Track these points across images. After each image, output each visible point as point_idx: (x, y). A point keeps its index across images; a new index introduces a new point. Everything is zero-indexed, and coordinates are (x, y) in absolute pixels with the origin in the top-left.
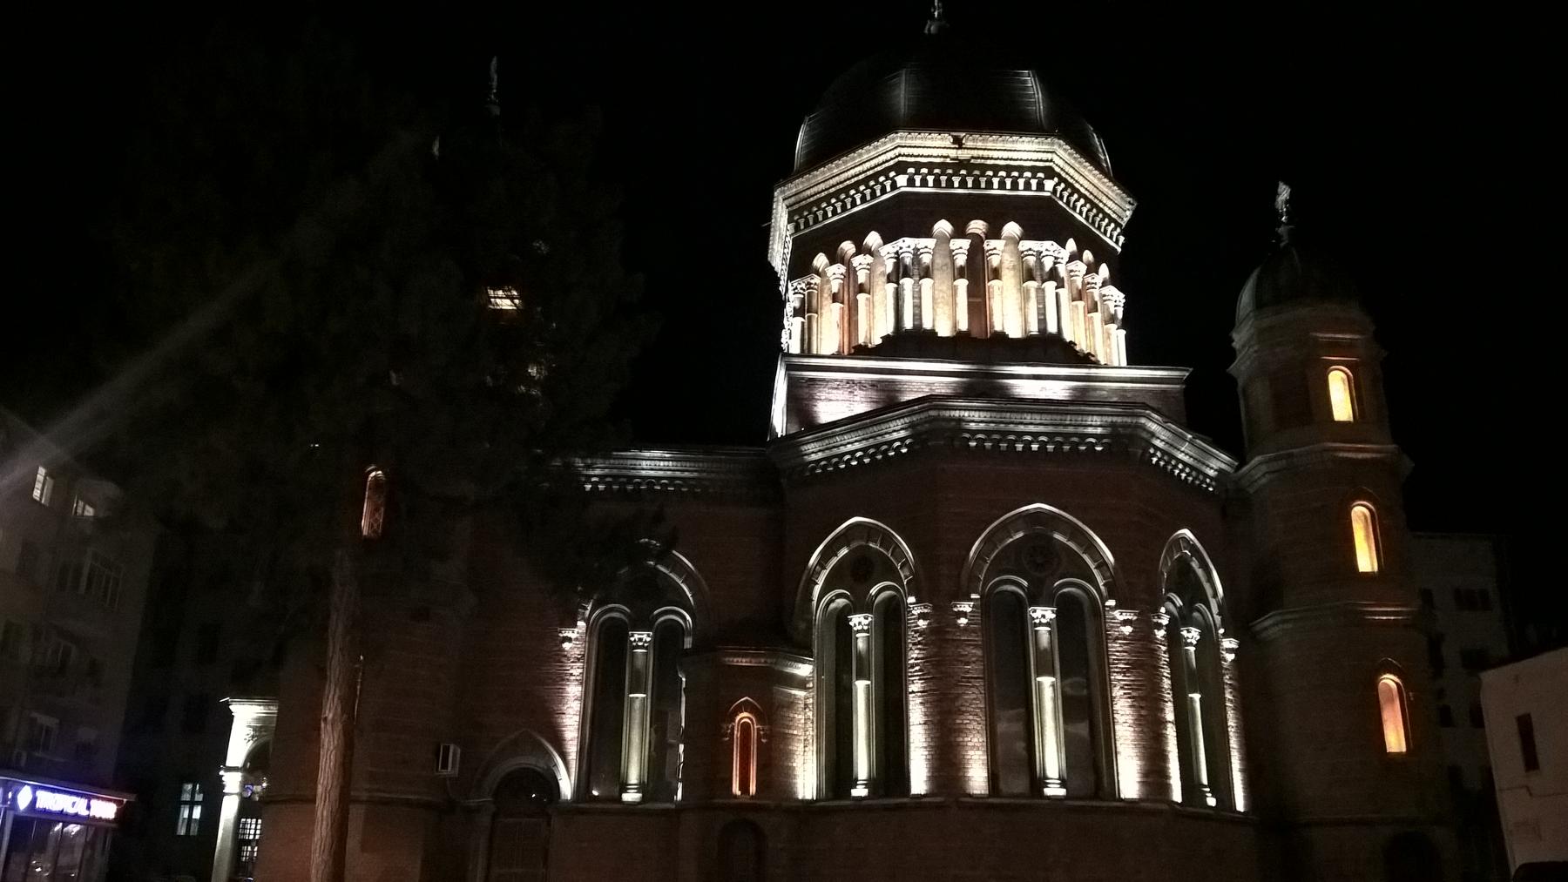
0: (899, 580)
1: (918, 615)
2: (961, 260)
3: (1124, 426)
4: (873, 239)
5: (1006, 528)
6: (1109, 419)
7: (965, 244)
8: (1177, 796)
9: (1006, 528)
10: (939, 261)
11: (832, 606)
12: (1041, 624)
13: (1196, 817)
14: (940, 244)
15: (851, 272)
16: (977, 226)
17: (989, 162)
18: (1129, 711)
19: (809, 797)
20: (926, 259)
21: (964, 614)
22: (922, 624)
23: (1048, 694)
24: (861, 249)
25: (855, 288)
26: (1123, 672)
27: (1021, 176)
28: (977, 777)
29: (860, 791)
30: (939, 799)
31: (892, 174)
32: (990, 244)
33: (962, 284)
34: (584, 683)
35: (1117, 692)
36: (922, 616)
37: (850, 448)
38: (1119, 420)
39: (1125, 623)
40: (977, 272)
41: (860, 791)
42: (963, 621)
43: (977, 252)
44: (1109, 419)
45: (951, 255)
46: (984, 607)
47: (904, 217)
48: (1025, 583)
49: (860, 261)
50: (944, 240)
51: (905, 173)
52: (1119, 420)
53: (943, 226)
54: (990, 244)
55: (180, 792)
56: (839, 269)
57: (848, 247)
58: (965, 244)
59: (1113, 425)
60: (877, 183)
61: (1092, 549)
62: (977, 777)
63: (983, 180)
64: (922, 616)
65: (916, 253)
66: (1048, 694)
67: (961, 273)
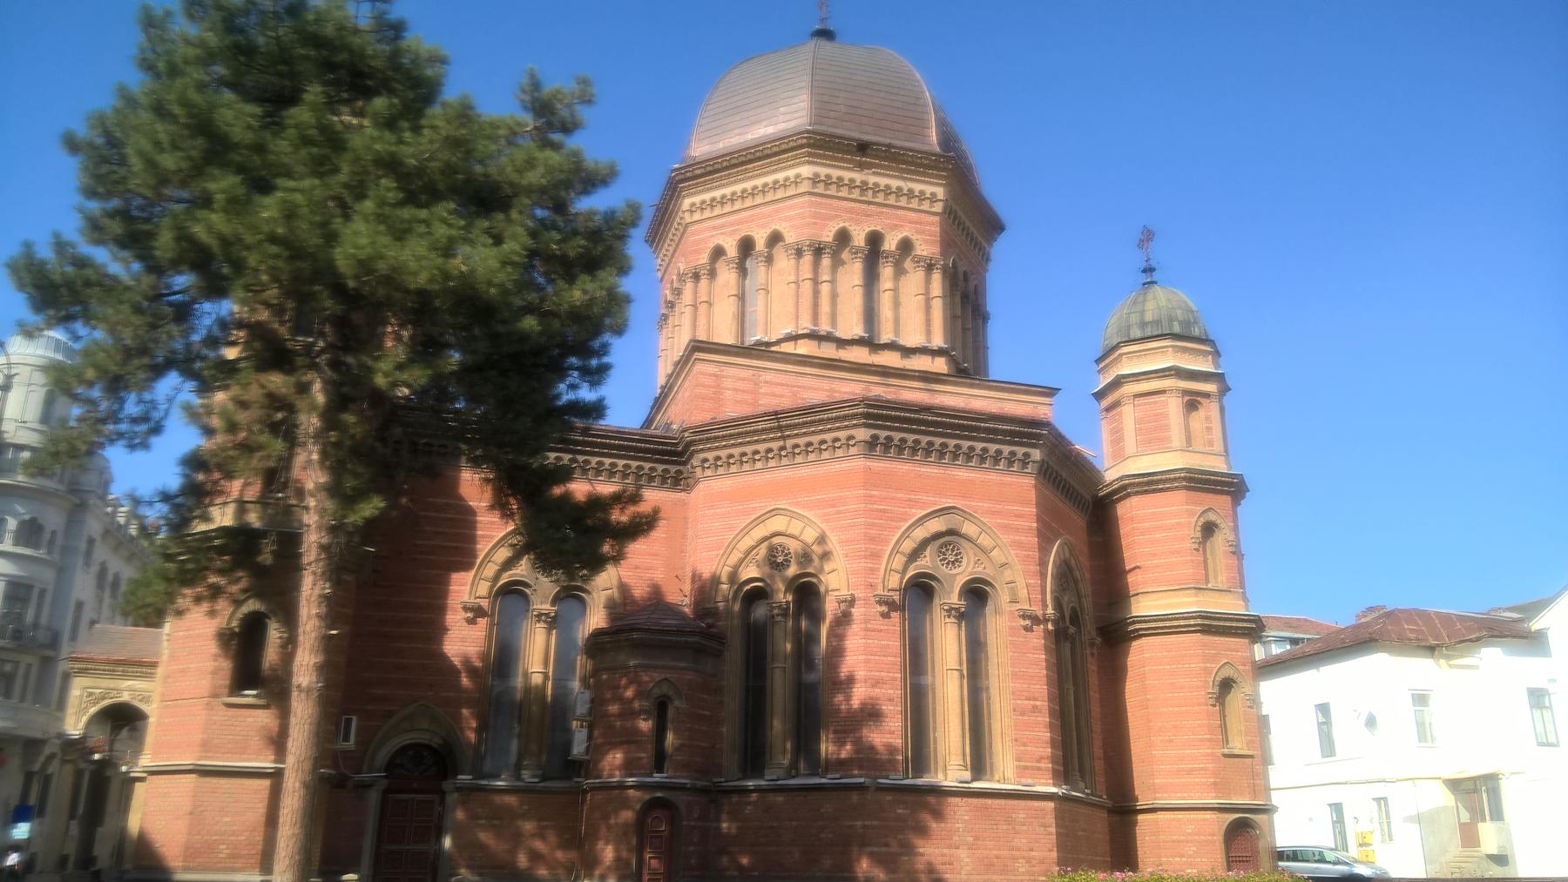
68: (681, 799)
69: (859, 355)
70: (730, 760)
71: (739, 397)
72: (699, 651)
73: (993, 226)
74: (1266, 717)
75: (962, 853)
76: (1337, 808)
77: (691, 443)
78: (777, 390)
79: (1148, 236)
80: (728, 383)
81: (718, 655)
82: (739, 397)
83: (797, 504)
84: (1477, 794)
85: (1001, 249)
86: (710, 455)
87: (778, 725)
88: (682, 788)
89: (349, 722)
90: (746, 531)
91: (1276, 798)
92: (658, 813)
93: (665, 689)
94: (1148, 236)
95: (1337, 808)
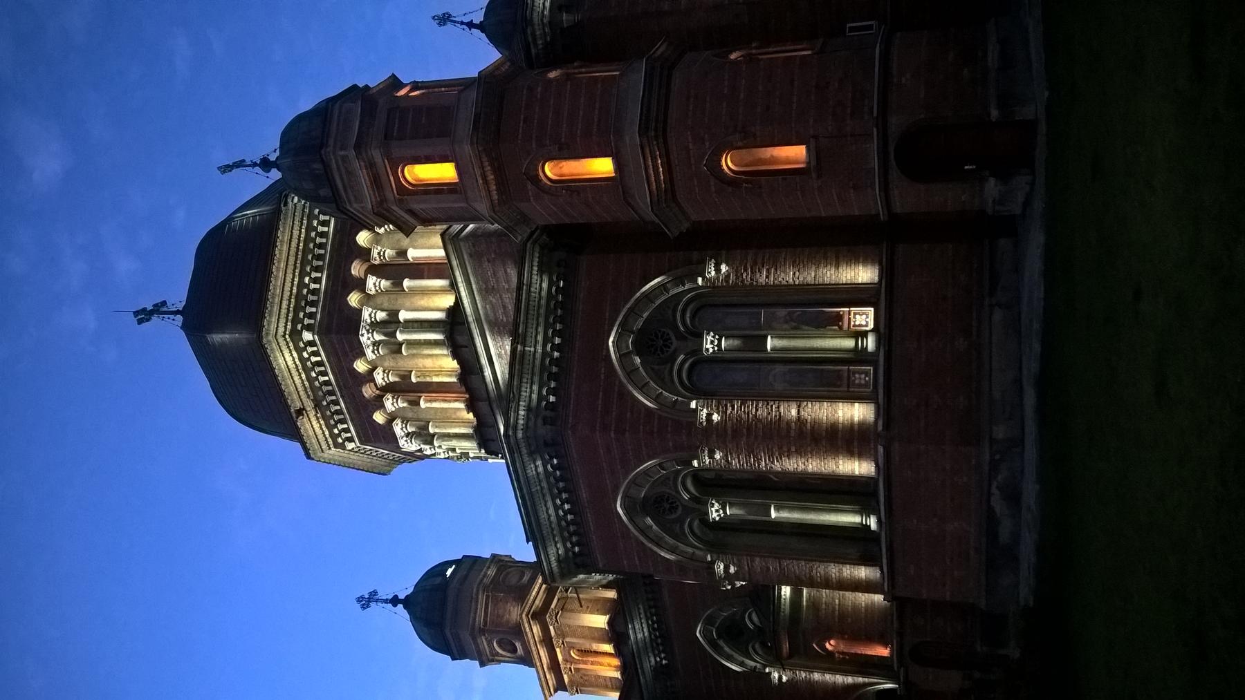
0: (678, 472)
1: (710, 459)
2: (385, 284)
3: (529, 445)
4: (360, 366)
5: (631, 372)
6: (526, 458)
7: (371, 281)
8: (878, 598)
9: (631, 372)
10: (386, 305)
11: (697, 531)
12: (719, 345)
13: (892, 584)
14: (369, 300)
15: (389, 388)
16: (357, 269)
17: (295, 291)
18: (793, 461)
19: (877, 271)
20: (381, 315)
21: (709, 415)
22: (718, 456)
23: (785, 515)
24: (369, 377)
25: (404, 387)
26: (759, 461)
27: (315, 229)
28: (857, 412)
29: (873, 523)
30: (881, 449)
31: (302, 345)
32: (376, 258)
33: (407, 283)
34: (775, 264)
35: (777, 466)
36: (711, 456)
37: (551, 511)
38: (524, 451)
39: (718, 270)
40: (398, 270)
41: (873, 523)
42: (716, 417)
43: (379, 270)
44: (526, 458)
45: (380, 293)
46: (704, 394)
47: (340, 330)
48: (682, 357)
49: (379, 377)
50: (368, 299)
51: (300, 333)
52: (524, 451)
53: (354, 299)
54: (376, 258)
55: (878, 342)
56: (390, 403)
57: (368, 391)
58: (371, 281)
59: (531, 454)
60: (309, 359)
61: (648, 296)
62: (857, 412)
63: (310, 298)
64: (711, 456)
65: (375, 326)
66: (785, 515)
67: (398, 284)
89: (852, 29)
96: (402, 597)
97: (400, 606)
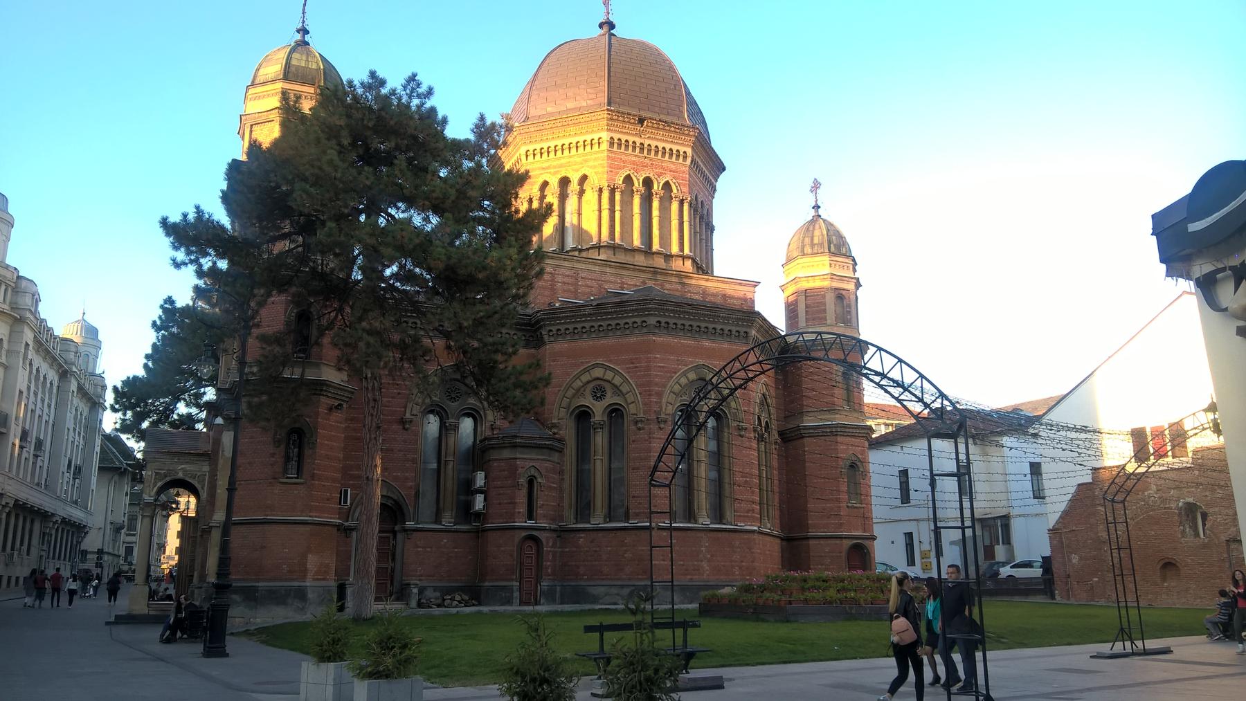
68: (543, 536)
69: (640, 260)
70: (569, 514)
71: (566, 287)
72: (551, 449)
73: (718, 167)
74: (1162, 261)
75: (705, 564)
76: (909, 536)
77: (543, 320)
78: (589, 283)
79: (816, 186)
80: (559, 279)
81: (560, 451)
82: (566, 287)
83: (610, 361)
84: (58, 570)
85: (722, 182)
86: (554, 329)
87: (55, 391)
88: (544, 529)
89: (346, 492)
90: (578, 377)
91: (877, 530)
92: (530, 543)
93: (533, 472)
94: (816, 186)
95: (909, 536)
96: (307, 38)
97: (298, 37)
